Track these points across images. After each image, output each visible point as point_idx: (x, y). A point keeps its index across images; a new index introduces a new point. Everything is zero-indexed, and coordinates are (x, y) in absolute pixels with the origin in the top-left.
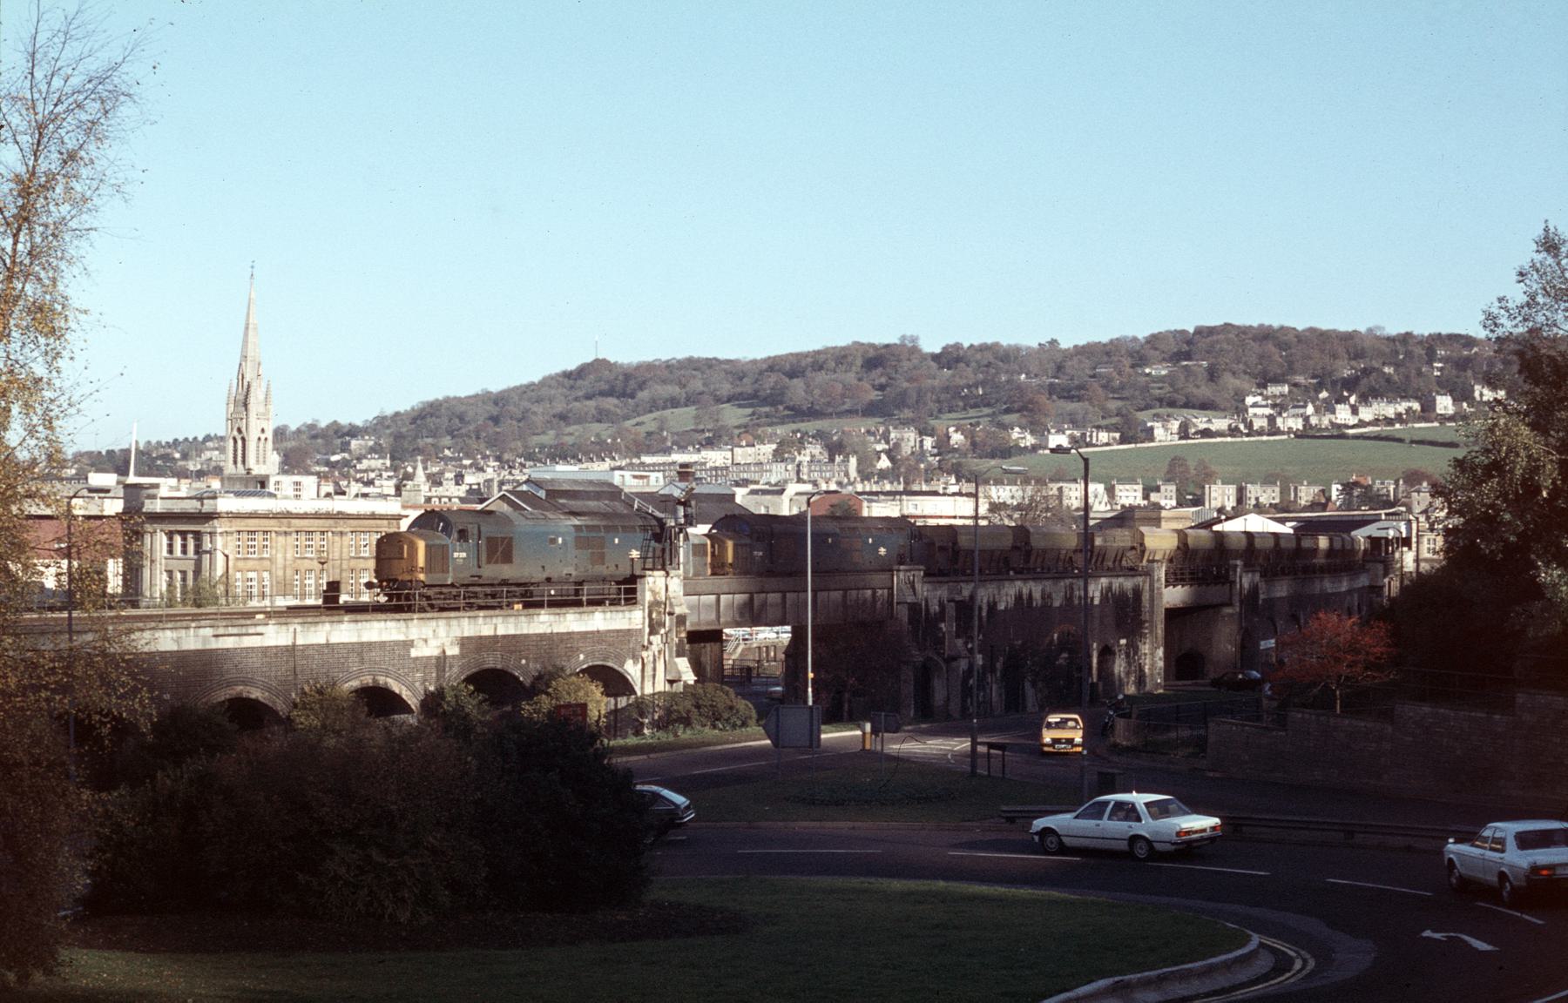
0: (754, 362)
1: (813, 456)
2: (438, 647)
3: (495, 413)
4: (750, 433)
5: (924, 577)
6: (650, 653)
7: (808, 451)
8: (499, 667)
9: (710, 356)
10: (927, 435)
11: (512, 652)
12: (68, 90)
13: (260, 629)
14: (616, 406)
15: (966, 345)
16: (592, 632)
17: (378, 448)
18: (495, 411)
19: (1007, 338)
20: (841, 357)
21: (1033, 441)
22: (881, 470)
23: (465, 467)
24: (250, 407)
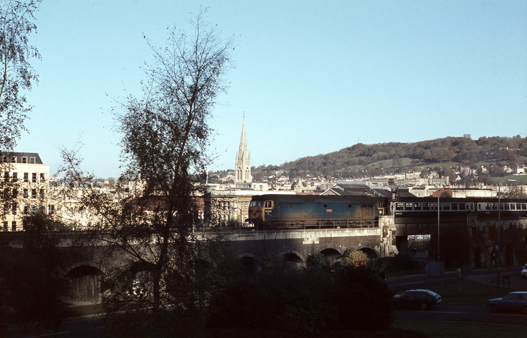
0: (413, 144)
1: (434, 176)
2: (312, 241)
3: (324, 162)
4: (412, 168)
5: (478, 218)
6: (383, 244)
7: (432, 175)
8: (332, 248)
9: (398, 142)
10: (474, 169)
11: (336, 243)
12: (207, 58)
13: (253, 234)
14: (365, 159)
15: (487, 137)
16: (364, 236)
17: (285, 174)
18: (324, 161)
19: (502, 134)
20: (443, 142)
21: (512, 171)
22: (458, 181)
23: (314, 180)
24: (243, 160)
